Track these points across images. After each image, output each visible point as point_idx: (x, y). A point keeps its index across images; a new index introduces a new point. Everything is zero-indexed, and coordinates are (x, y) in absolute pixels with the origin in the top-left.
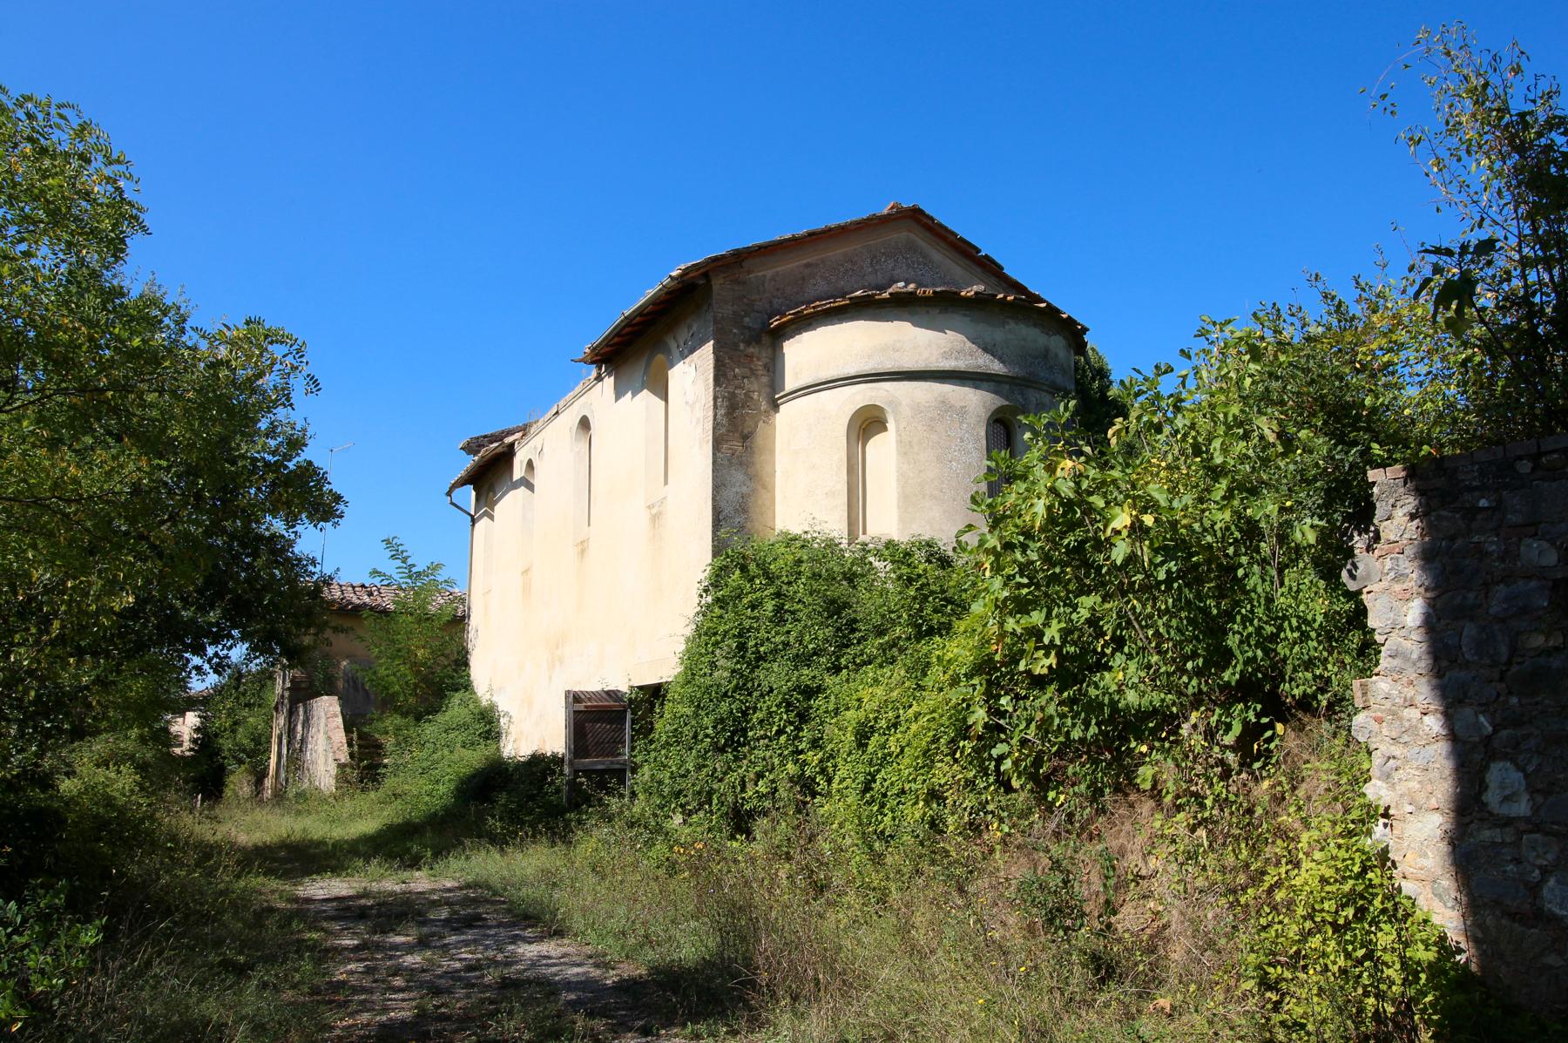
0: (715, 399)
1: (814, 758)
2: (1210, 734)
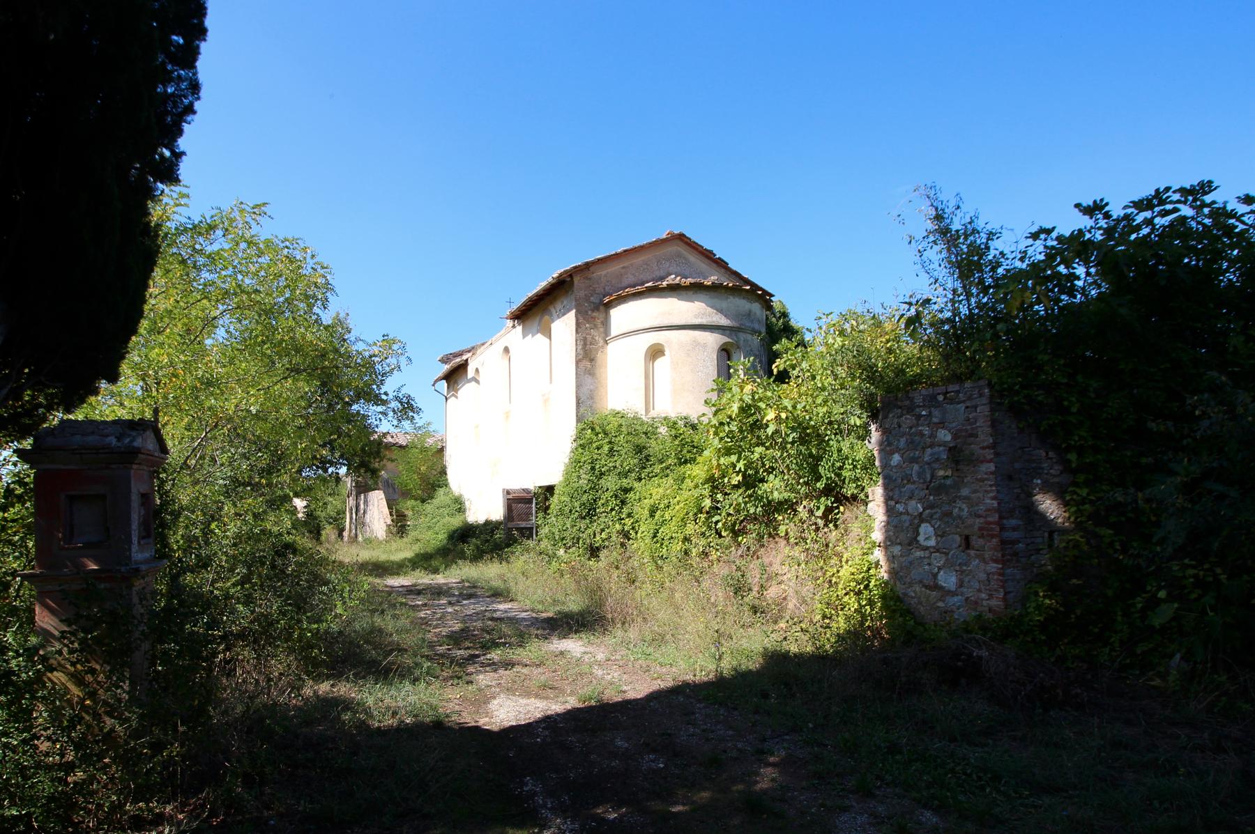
1: (628, 522)
2: (811, 512)
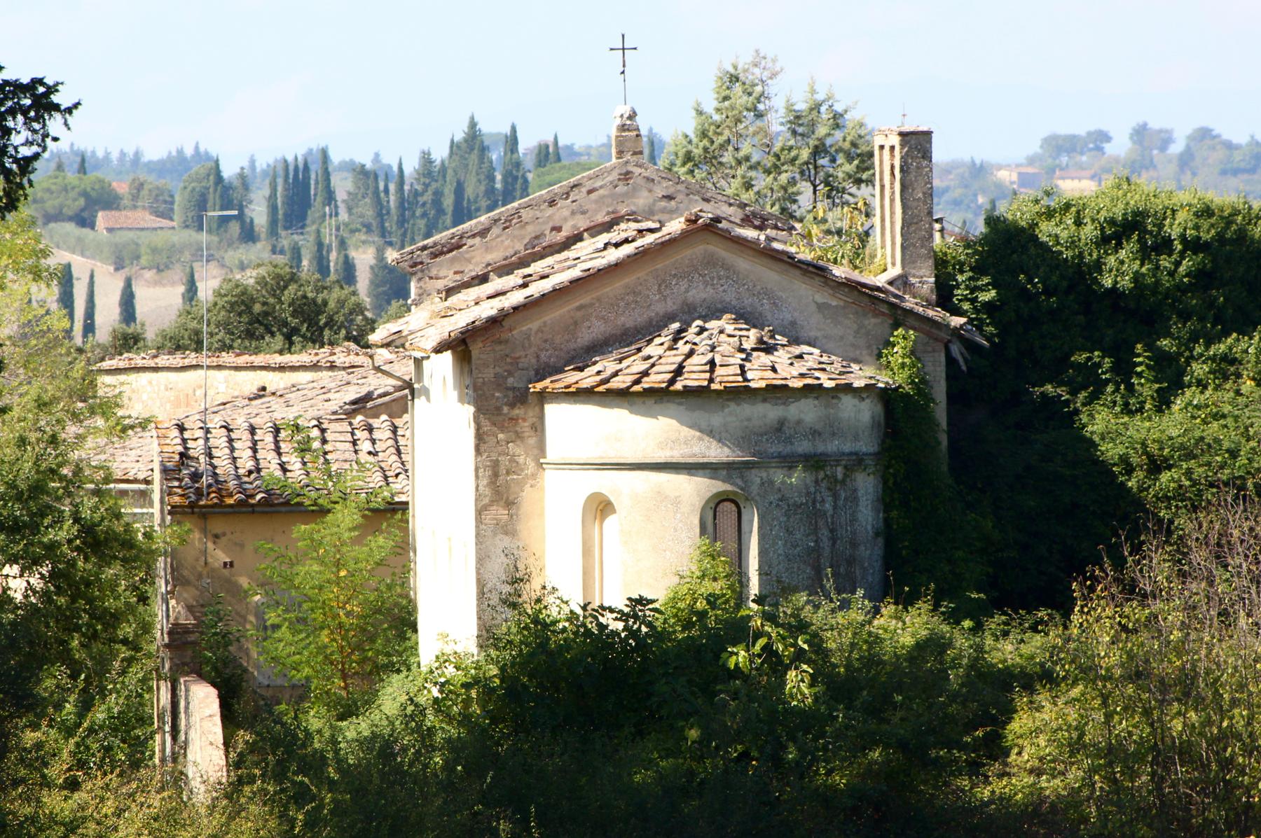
0: (477, 469)
